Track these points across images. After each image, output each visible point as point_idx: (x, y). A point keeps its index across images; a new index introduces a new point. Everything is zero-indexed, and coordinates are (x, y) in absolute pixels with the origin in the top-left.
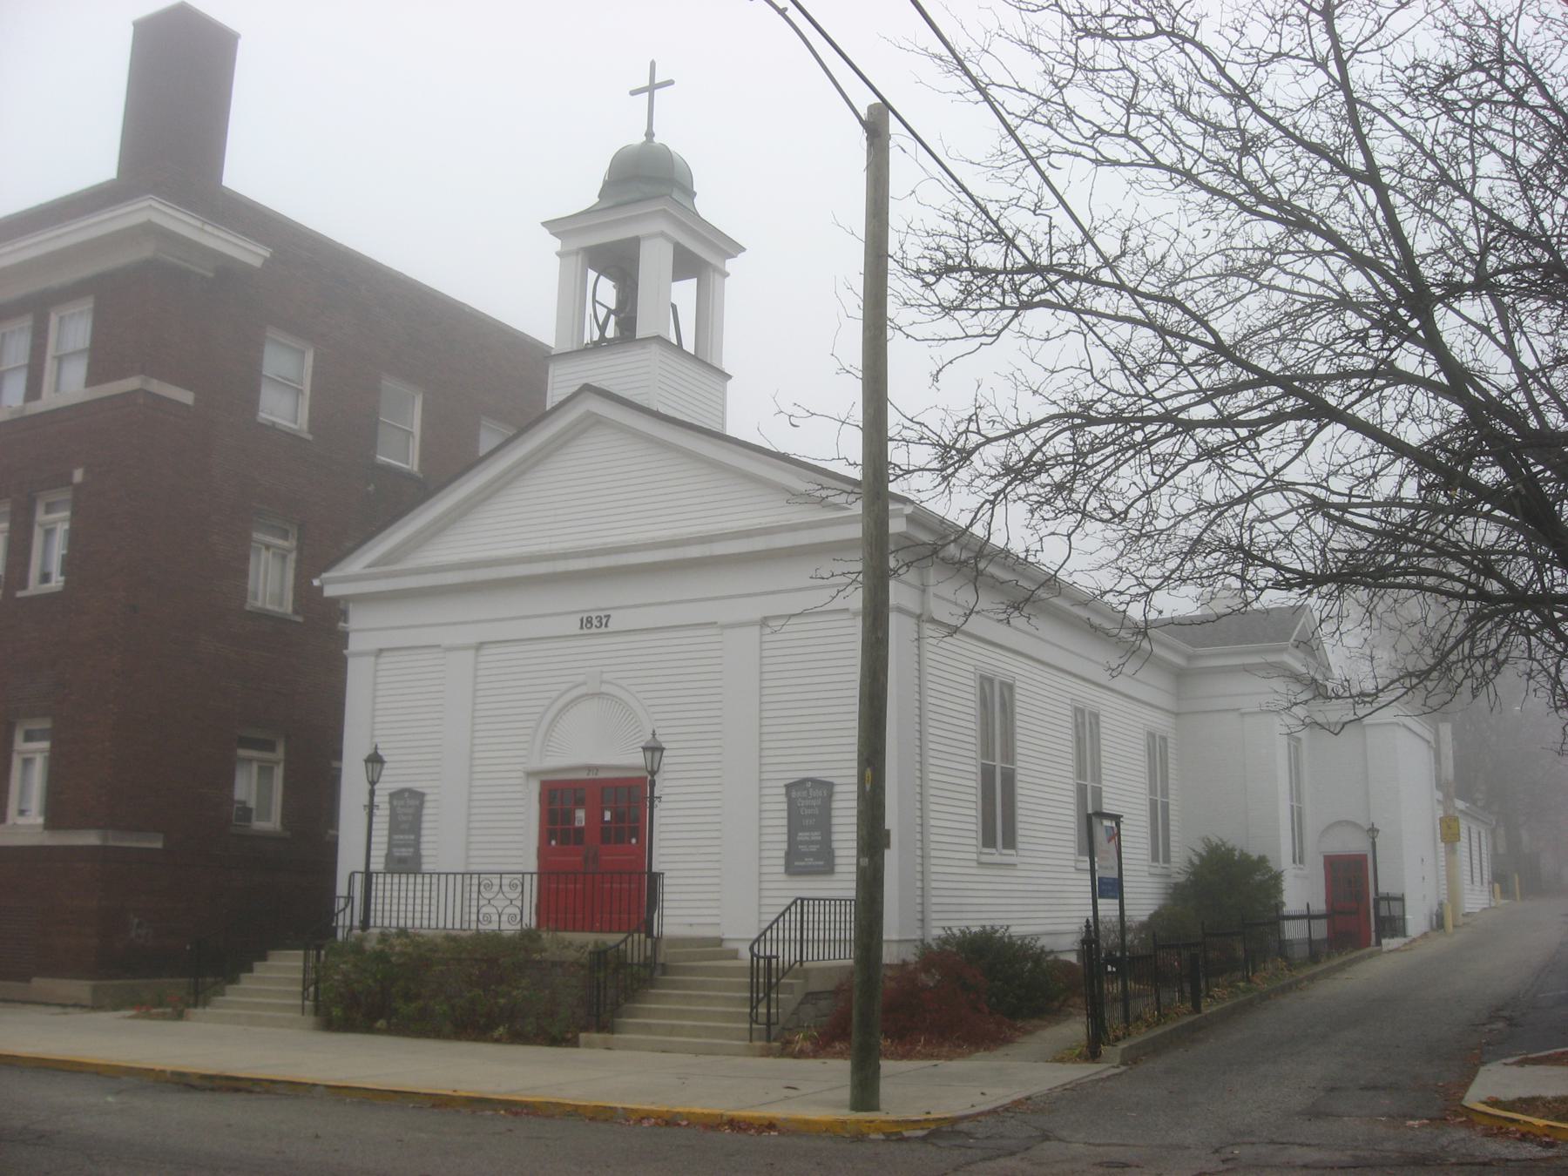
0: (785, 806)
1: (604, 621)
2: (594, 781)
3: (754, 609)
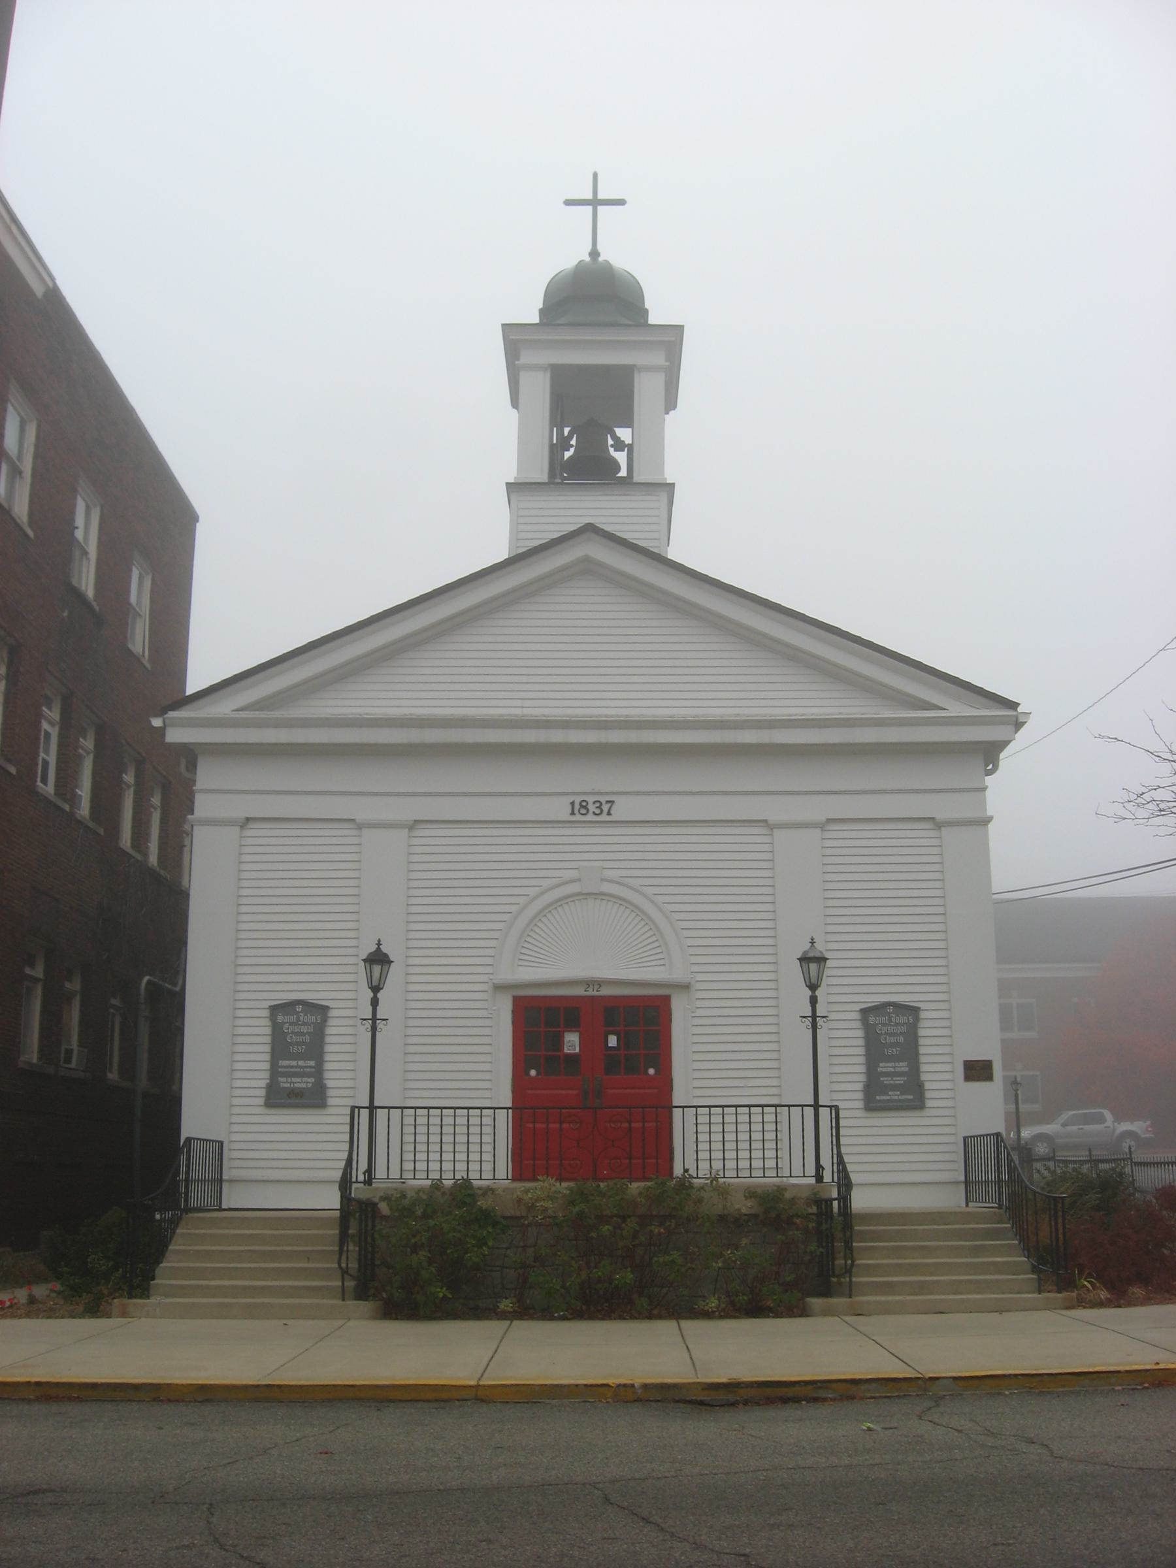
0: (268, 1031)
1: (606, 808)
2: (593, 999)
3: (818, 809)
